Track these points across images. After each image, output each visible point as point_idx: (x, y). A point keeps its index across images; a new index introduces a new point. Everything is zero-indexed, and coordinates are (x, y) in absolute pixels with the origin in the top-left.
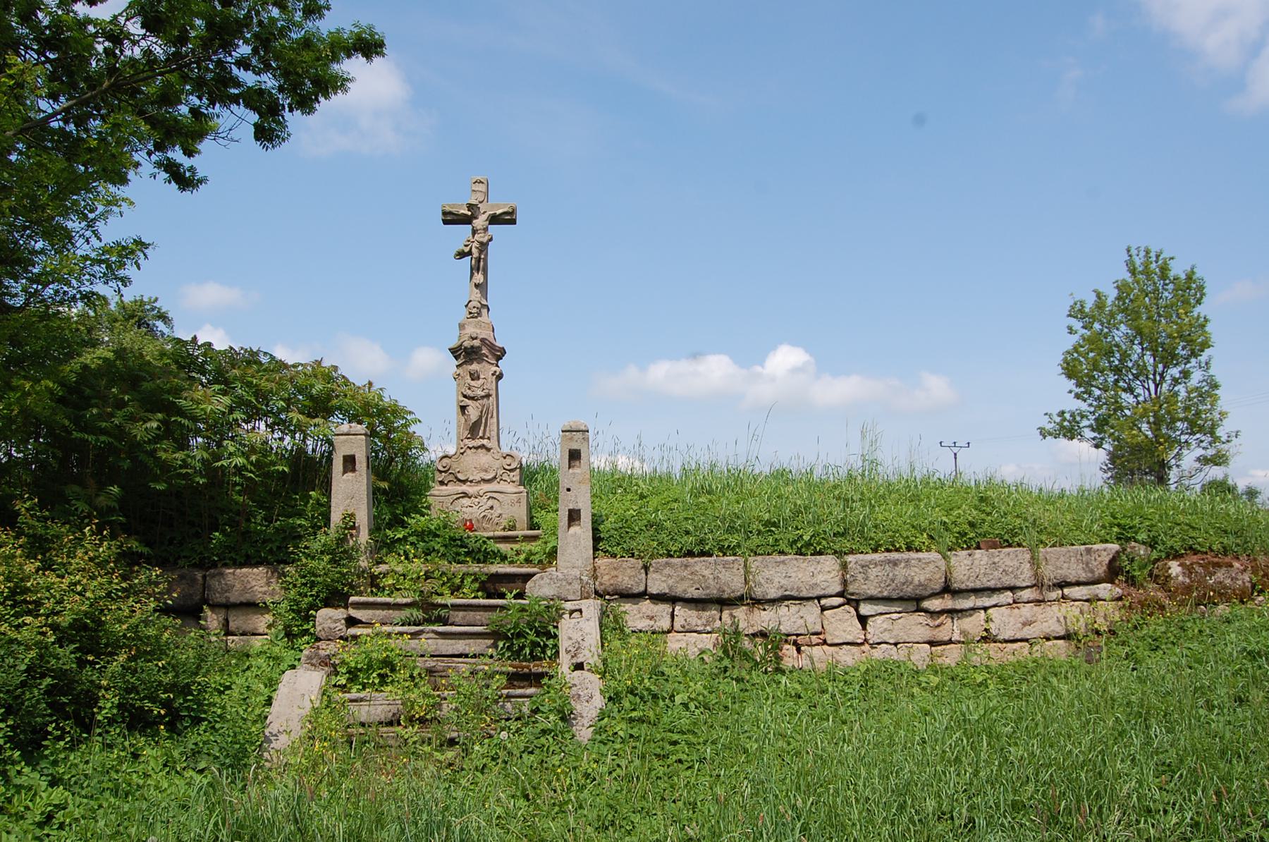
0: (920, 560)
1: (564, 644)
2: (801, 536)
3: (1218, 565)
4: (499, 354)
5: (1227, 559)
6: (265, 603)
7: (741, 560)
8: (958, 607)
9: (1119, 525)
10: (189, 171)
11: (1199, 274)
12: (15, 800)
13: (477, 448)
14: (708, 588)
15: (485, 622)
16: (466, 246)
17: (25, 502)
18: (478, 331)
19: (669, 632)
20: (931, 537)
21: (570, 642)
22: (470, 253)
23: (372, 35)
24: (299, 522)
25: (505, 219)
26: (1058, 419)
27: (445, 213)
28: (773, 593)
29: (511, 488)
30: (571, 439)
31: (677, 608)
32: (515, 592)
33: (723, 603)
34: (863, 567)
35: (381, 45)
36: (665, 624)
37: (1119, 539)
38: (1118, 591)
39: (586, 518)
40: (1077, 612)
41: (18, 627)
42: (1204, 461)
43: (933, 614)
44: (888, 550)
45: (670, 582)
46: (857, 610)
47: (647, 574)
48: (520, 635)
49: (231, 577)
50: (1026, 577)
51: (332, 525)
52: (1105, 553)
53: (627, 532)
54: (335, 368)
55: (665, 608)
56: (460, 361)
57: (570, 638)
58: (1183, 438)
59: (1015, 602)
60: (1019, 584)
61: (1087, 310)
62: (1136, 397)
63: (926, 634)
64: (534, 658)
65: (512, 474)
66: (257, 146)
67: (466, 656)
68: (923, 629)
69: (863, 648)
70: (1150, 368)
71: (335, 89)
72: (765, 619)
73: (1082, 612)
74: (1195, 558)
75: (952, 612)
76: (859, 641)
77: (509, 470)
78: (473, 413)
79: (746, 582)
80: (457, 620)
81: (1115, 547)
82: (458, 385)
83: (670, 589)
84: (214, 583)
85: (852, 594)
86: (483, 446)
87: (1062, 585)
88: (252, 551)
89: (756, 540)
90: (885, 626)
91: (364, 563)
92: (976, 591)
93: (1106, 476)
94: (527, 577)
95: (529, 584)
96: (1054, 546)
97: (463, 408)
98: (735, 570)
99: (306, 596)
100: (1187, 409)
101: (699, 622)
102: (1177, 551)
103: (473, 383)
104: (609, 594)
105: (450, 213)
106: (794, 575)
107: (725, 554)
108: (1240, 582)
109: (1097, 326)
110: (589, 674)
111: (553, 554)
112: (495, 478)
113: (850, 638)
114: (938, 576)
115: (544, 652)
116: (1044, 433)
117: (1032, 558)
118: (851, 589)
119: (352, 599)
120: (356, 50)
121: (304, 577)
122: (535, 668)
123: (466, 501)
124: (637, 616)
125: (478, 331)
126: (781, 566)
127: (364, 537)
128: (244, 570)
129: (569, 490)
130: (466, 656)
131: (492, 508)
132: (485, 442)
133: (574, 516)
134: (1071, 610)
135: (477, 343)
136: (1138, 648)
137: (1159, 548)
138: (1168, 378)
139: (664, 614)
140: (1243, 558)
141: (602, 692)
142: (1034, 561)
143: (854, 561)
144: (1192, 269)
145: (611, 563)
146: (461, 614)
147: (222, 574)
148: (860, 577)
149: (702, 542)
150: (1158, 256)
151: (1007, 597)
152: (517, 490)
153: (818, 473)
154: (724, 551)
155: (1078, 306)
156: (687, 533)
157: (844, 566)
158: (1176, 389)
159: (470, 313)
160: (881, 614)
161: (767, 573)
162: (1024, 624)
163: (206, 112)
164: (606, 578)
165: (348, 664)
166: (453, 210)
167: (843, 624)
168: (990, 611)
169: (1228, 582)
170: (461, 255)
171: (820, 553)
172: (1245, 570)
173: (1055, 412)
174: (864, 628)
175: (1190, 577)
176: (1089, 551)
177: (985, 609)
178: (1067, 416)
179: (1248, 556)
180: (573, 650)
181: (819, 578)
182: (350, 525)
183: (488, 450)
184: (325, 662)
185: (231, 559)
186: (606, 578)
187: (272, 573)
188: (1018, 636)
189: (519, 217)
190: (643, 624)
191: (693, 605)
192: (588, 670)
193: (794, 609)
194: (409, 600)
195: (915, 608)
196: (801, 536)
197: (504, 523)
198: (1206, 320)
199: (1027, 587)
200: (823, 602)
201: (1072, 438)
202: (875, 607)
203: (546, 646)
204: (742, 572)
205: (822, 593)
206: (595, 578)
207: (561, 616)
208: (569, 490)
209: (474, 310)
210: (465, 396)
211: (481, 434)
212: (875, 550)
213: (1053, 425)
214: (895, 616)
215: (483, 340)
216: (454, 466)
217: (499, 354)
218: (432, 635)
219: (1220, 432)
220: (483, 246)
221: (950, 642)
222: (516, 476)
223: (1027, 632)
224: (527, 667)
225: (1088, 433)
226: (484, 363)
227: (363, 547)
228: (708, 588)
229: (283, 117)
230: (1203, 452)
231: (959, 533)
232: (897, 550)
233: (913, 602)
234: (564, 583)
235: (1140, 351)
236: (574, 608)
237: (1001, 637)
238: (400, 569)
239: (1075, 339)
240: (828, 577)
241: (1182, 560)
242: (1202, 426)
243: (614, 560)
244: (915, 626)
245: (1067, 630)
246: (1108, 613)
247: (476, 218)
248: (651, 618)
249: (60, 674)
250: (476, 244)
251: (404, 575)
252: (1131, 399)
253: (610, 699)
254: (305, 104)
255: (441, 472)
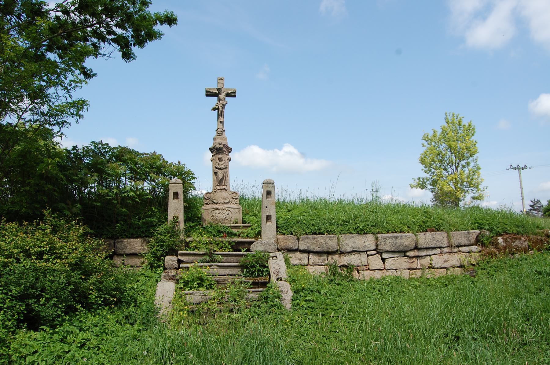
0: (406, 236)
1: (272, 271)
2: (359, 227)
3: (516, 239)
4: (230, 150)
5: (519, 236)
6: (140, 254)
7: (336, 236)
8: (420, 255)
9: (478, 223)
10: (89, 70)
11: (473, 124)
12: (68, 337)
13: (221, 190)
14: (323, 247)
15: (235, 261)
16: (217, 106)
17: (47, 211)
18: (222, 141)
19: (307, 265)
20: (409, 227)
21: (275, 269)
22: (218, 109)
23: (172, 15)
24: (153, 220)
25: (232, 95)
26: (417, 181)
27: (207, 92)
28: (349, 250)
29: (235, 206)
30: (268, 186)
31: (310, 255)
32: (245, 249)
33: (329, 253)
34: (384, 239)
35: (175, 20)
36: (306, 262)
37: (478, 228)
38: (480, 248)
39: (274, 219)
40: (464, 257)
41: (55, 264)
42: (474, 198)
43: (411, 258)
44: (392, 232)
45: (308, 245)
46: (381, 256)
47: (298, 242)
48: (254, 266)
49: (126, 243)
50: (445, 243)
51: (168, 221)
52: (475, 234)
53: (289, 225)
54: (161, 155)
55: (305, 256)
56: (214, 154)
57: (274, 268)
58: (466, 189)
59: (441, 253)
60: (443, 246)
61: (429, 137)
62: (448, 172)
63: (407, 265)
64: (259, 276)
65: (236, 200)
66: (122, 60)
67: (225, 275)
68: (406, 264)
69: (383, 271)
70: (454, 161)
71: (156, 38)
72: (345, 260)
73: (466, 257)
74: (507, 236)
75: (417, 257)
76: (382, 268)
77: (235, 199)
78: (220, 175)
79: (338, 245)
80: (223, 261)
81: (478, 231)
82: (213, 163)
83: (308, 248)
84: (118, 245)
85: (380, 250)
86: (224, 189)
87: (459, 246)
88: (134, 232)
89: (340, 228)
90: (392, 262)
91: (182, 237)
92: (427, 249)
93: (433, 203)
94: (252, 243)
95: (252, 246)
96: (455, 231)
97: (215, 173)
98: (334, 240)
99: (159, 251)
100: (468, 177)
101: (319, 261)
102: (500, 233)
103: (220, 163)
104: (283, 250)
105: (209, 92)
106: (357, 242)
107: (329, 234)
108: (524, 245)
109: (433, 144)
110: (285, 282)
111: (259, 233)
112: (229, 202)
113: (378, 267)
114: (413, 243)
115: (262, 273)
116: (412, 187)
117: (448, 236)
118: (379, 248)
119: (180, 252)
120: (165, 22)
121: (158, 243)
122: (261, 280)
123: (217, 212)
124: (295, 258)
125: (222, 141)
126: (352, 238)
127: (182, 226)
128: (132, 240)
129: (266, 207)
130: (225, 275)
131: (228, 214)
132: (225, 187)
133: (269, 218)
134: (463, 256)
135: (221, 146)
136: (490, 271)
137: (493, 232)
138: (460, 165)
139: (305, 258)
140: (525, 236)
141: (291, 290)
142: (448, 237)
143: (381, 236)
144: (471, 121)
145: (284, 237)
146: (225, 258)
147: (122, 242)
148: (383, 243)
149: (319, 229)
150: (457, 116)
151: (438, 251)
152: (238, 207)
153: (312, 200)
154: (329, 232)
155: (426, 136)
156: (313, 225)
157: (377, 239)
158: (464, 169)
159: (218, 134)
160: (391, 258)
161: (347, 242)
162: (445, 262)
163: (99, 46)
164: (282, 243)
165: (184, 279)
166: (211, 91)
167: (376, 262)
168: (432, 256)
169: (520, 245)
170: (214, 109)
171: (366, 234)
172: (526, 241)
173: (416, 178)
174: (384, 263)
175: (506, 243)
176: (468, 233)
177: (430, 256)
178: (421, 180)
179: (526, 235)
180: (276, 272)
181: (367, 243)
182: (176, 220)
183: (226, 190)
184: (172, 278)
185: (125, 235)
186: (282, 243)
187: (144, 241)
188: (442, 266)
189: (237, 94)
190: (296, 262)
191: (317, 254)
192: (284, 281)
193: (357, 256)
194: (204, 252)
195: (403, 256)
196: (359, 227)
197: (233, 221)
198: (476, 142)
199: (446, 247)
200: (368, 253)
201: (422, 189)
202: (388, 255)
203: (263, 271)
204: (337, 241)
205: (368, 249)
206: (278, 243)
207: (269, 258)
208: (266, 207)
209: (220, 133)
210: (216, 168)
211: (223, 184)
212: (388, 232)
213: (415, 183)
214: (396, 258)
215: (224, 145)
216: (212, 197)
217: (230, 150)
218: (216, 267)
219: (480, 187)
220: (224, 106)
221: (417, 269)
222: (237, 201)
223: (446, 265)
224: (258, 280)
225: (429, 187)
226: (224, 155)
227: (182, 230)
228: (323, 247)
229: (131, 48)
230: (474, 195)
231: (419, 226)
232: (396, 232)
233: (403, 253)
234: (268, 245)
235: (450, 154)
236: (273, 255)
237: (436, 267)
238: (198, 239)
239: (424, 149)
240: (370, 243)
241: (502, 237)
242: (473, 185)
243: (284, 236)
244: (403, 262)
245: (461, 264)
246: (475, 258)
247: (221, 94)
248: (300, 260)
249: (75, 284)
250: (221, 105)
251: (200, 242)
252: (446, 173)
253: (294, 292)
254: (141, 43)
255: (206, 199)
